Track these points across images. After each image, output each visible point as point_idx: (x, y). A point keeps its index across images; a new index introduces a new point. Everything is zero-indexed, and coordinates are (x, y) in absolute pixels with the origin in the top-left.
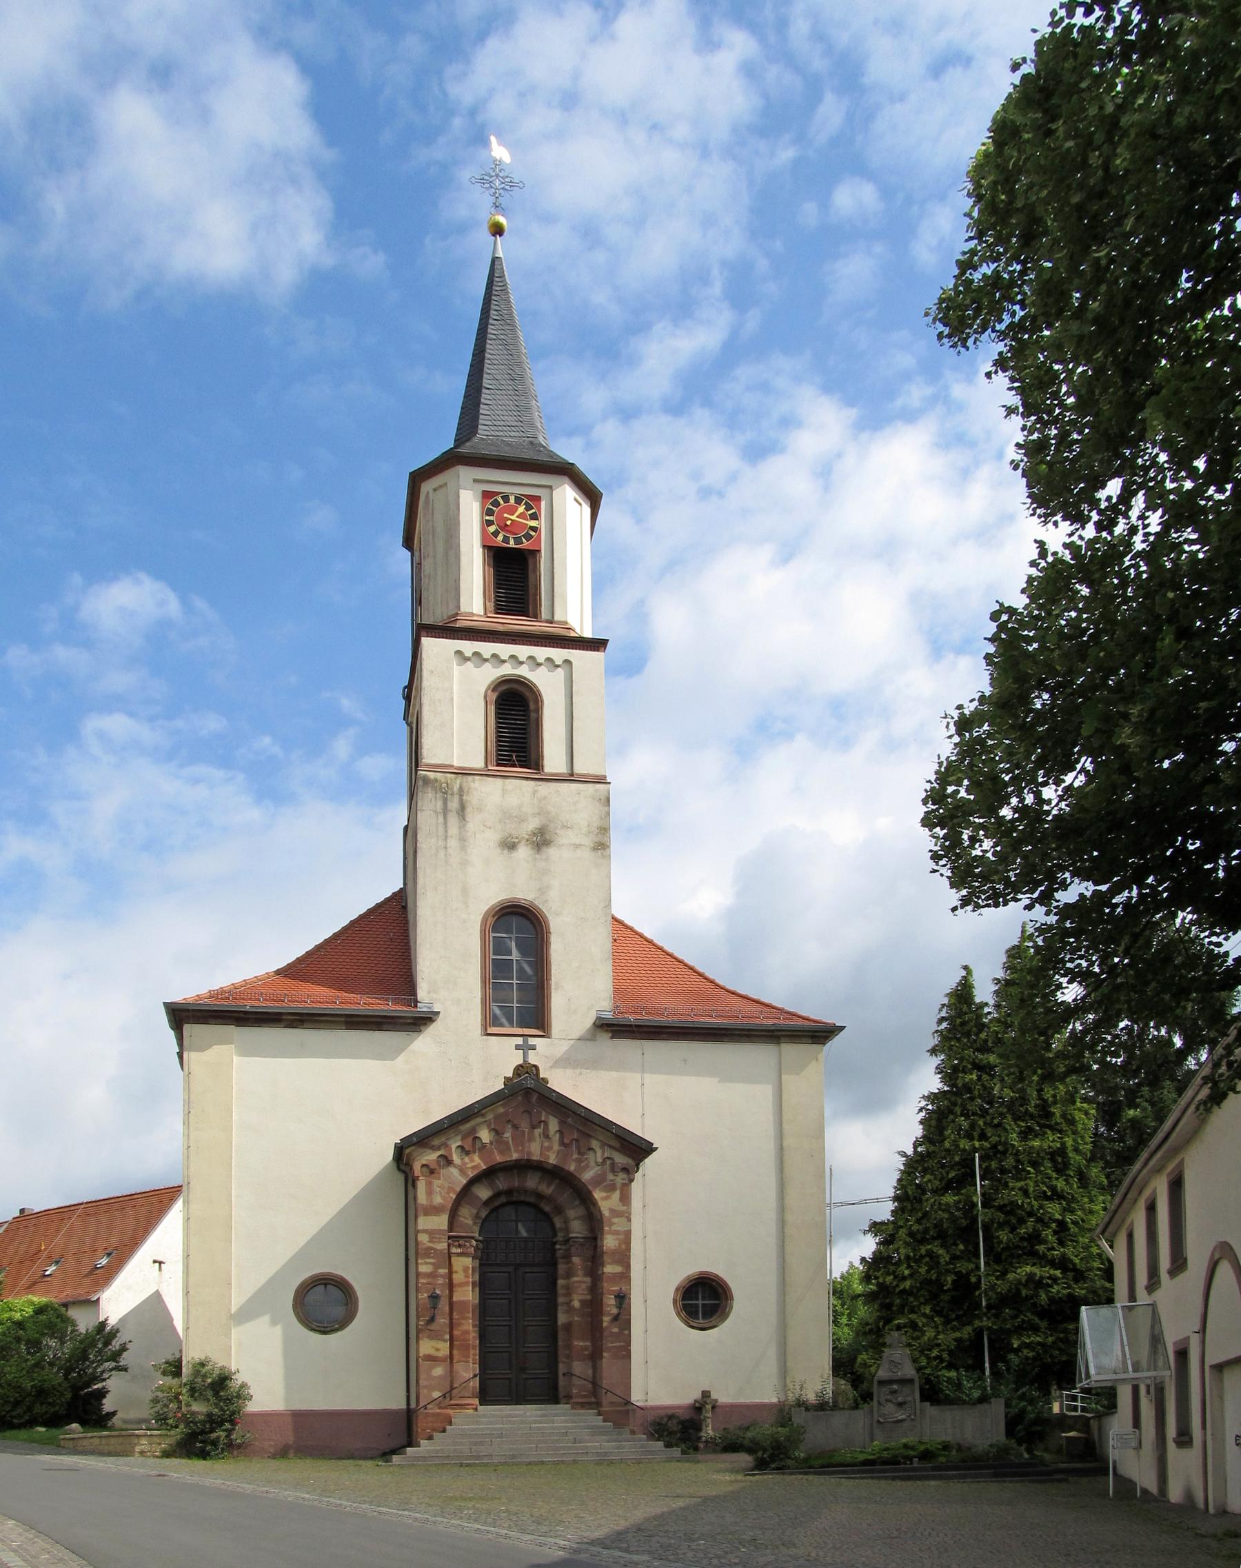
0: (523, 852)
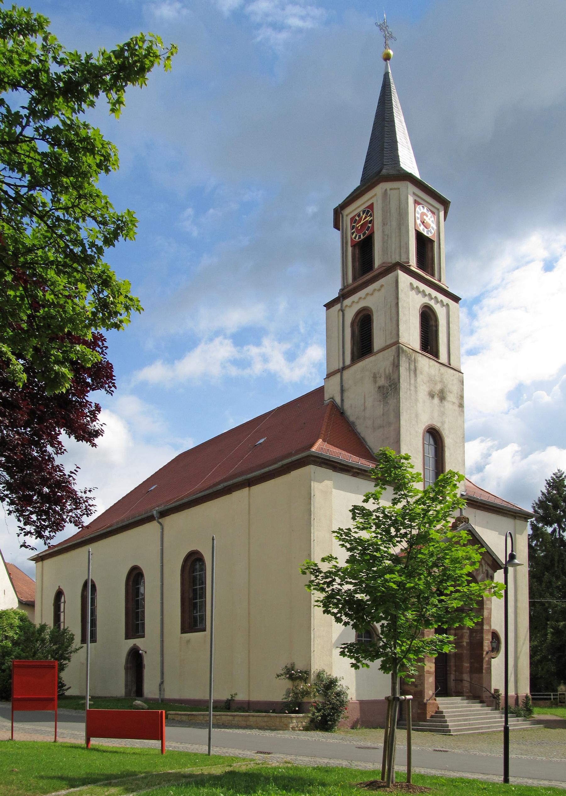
0: (436, 400)
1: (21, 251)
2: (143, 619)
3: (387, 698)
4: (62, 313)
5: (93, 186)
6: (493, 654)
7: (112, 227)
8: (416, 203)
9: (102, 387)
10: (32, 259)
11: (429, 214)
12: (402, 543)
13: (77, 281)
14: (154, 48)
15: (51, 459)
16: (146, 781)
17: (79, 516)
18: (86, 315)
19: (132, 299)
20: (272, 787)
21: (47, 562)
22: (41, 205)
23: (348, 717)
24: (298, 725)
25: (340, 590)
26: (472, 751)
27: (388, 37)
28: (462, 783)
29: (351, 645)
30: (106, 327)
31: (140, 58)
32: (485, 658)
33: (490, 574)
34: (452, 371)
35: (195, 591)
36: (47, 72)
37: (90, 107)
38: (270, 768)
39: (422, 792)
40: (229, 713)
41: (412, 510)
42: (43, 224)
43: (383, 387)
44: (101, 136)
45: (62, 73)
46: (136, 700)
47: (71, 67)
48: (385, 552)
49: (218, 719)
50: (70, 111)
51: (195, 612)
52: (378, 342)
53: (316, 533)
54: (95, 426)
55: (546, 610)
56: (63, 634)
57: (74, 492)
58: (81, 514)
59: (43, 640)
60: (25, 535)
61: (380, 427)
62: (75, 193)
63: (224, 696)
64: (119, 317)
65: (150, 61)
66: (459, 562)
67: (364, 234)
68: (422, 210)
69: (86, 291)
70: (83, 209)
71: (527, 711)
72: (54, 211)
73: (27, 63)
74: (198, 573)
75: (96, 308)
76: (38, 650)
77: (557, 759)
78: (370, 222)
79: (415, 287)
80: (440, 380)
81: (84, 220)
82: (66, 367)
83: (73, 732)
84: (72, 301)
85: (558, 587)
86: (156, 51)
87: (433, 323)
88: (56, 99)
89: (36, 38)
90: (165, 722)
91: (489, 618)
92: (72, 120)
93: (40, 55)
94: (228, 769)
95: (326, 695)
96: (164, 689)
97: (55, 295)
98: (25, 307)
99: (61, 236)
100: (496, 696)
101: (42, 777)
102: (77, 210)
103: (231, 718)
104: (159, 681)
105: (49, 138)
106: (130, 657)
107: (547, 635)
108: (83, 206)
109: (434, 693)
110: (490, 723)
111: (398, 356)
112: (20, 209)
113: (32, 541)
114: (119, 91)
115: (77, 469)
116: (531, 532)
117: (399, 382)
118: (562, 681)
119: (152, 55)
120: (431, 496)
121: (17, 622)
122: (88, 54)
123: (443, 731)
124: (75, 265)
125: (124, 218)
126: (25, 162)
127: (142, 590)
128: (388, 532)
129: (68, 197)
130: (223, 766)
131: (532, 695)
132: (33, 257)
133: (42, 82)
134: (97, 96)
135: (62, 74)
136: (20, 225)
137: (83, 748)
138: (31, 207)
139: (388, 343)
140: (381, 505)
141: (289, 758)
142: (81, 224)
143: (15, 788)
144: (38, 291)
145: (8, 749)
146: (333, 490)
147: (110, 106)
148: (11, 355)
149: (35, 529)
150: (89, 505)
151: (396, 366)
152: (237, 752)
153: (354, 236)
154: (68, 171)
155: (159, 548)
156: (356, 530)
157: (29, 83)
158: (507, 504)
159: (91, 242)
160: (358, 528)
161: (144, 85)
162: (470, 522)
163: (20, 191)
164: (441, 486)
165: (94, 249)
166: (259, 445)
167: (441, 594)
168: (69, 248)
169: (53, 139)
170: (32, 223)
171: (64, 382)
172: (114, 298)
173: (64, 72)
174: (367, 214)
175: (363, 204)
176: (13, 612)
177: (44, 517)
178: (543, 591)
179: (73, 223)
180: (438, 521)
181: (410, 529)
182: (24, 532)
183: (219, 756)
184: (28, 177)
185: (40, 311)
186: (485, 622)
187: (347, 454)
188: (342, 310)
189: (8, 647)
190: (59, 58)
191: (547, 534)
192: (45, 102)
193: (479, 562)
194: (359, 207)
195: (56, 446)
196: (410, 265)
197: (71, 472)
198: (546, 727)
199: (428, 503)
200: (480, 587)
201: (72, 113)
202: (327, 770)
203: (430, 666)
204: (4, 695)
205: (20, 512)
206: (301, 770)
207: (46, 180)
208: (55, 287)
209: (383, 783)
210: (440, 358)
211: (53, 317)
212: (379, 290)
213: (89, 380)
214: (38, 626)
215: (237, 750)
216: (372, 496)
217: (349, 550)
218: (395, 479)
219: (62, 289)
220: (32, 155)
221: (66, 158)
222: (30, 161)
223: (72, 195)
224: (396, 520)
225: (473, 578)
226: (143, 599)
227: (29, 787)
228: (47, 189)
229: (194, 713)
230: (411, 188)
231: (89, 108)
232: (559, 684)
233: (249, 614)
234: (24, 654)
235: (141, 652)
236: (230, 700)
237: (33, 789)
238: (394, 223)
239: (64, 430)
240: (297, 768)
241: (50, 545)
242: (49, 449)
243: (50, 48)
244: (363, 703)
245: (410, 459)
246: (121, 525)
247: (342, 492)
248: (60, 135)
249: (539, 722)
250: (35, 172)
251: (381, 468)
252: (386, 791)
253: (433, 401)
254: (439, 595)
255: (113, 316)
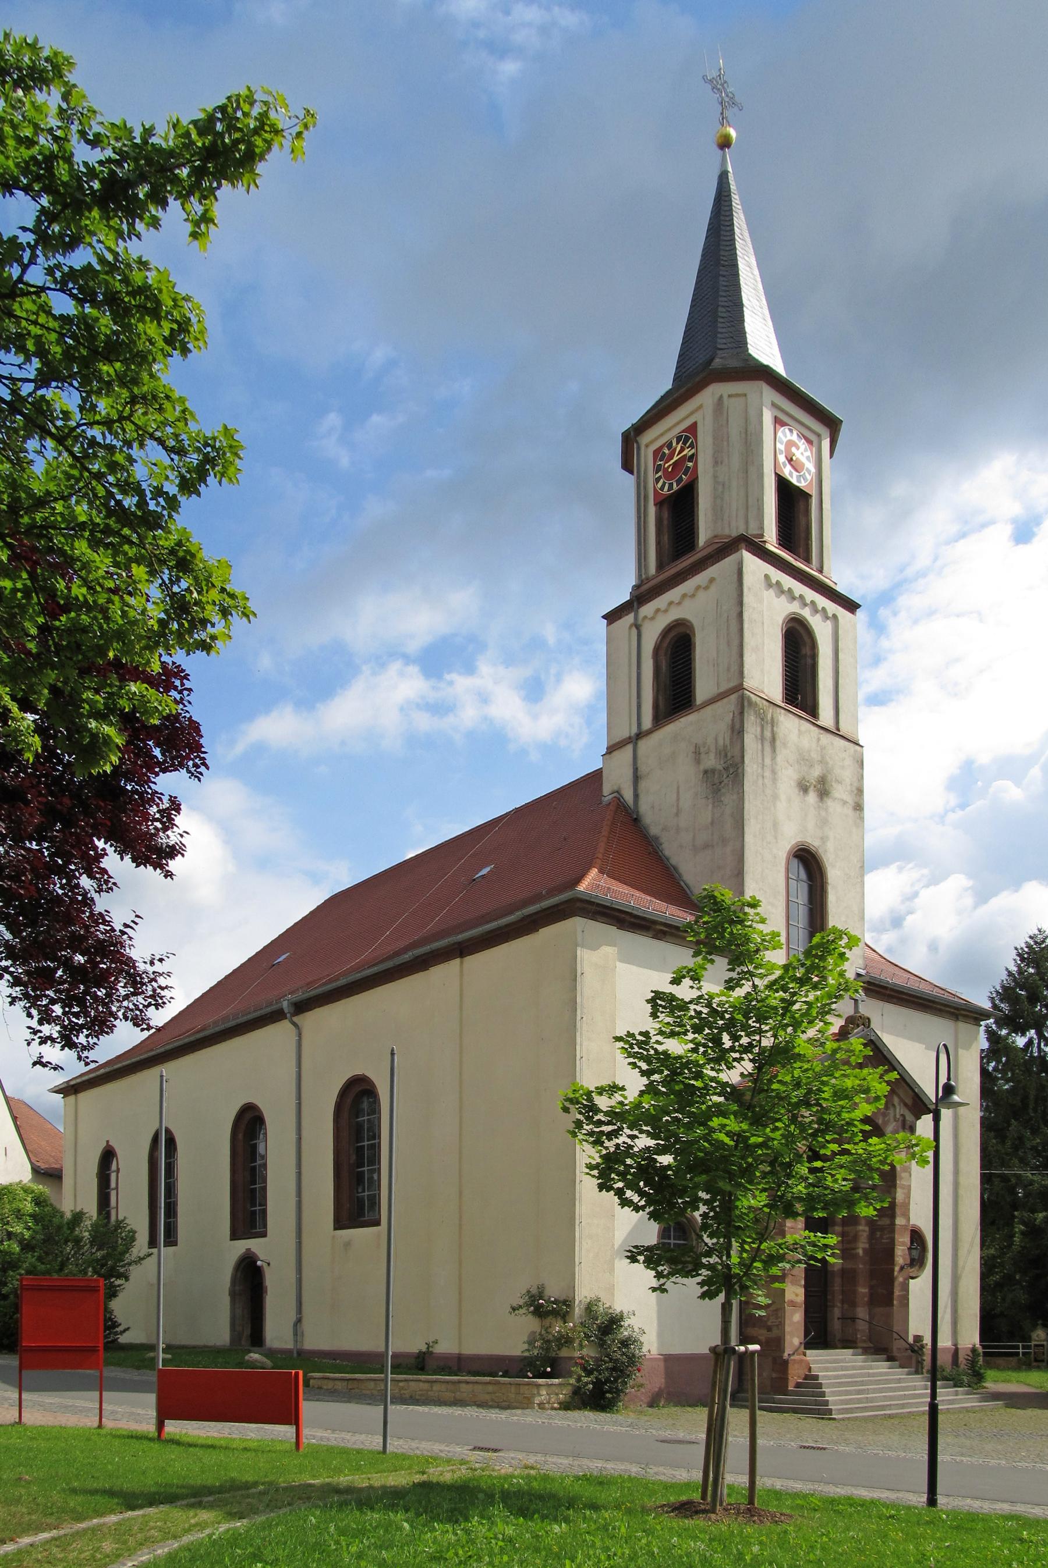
0: (812, 797)
1: (24, 504)
2: (264, 1203)
3: (713, 1350)
4: (102, 621)
5: (158, 379)
6: (913, 1271)
7: (194, 458)
8: (778, 422)
9: (181, 765)
10: (45, 519)
11: (802, 444)
12: (742, 1063)
13: (130, 560)
14: (272, 114)
15: (88, 902)
16: (266, 1499)
17: (141, 1007)
18: (147, 625)
19: (233, 594)
20: (498, 1511)
21: (84, 1096)
22: (61, 416)
23: (642, 1385)
24: (550, 1399)
25: (631, 1147)
26: (870, 1448)
27: (727, 104)
28: (851, 1505)
29: (649, 1249)
30: (186, 648)
31: (245, 135)
32: (897, 1277)
33: (908, 1123)
34: (843, 742)
35: (360, 1150)
36: (68, 159)
37: (151, 228)
38: (496, 1477)
39: (776, 1522)
40: (423, 1377)
41: (763, 1000)
42: (65, 454)
43: (713, 771)
44: (171, 284)
45: (97, 162)
46: (250, 1352)
47: (114, 152)
48: (713, 1079)
49: (402, 1388)
50: (112, 235)
51: (360, 1190)
52: (704, 686)
53: (585, 1043)
54: (168, 837)
55: (1012, 1191)
56: (116, 1230)
57: (130, 962)
58: (146, 1003)
59: (78, 1241)
60: (40, 1044)
61: (707, 846)
62: (125, 394)
63: (415, 1345)
64: (210, 630)
65: (265, 140)
66: (846, 1097)
67: (678, 482)
68: (789, 437)
69: (147, 580)
70: (140, 423)
71: (975, 1376)
72: (84, 427)
73: (30, 143)
74: (366, 1118)
75: (166, 611)
76: (68, 1259)
77: (1027, 1465)
78: (691, 458)
79: (774, 581)
80: (819, 758)
81: (142, 445)
82: (111, 724)
83: (134, 1410)
84: (122, 597)
85: (1034, 1148)
86: (277, 122)
87: (806, 650)
88: (87, 214)
89: (49, 94)
90: (304, 1393)
91: (906, 1205)
92: (116, 255)
93: (55, 128)
94: (418, 1478)
95: (602, 1344)
96: (303, 1333)
97: (90, 588)
98: (34, 610)
99: (99, 476)
100: (916, 1347)
101: (74, 1491)
102: (129, 427)
103: (426, 1386)
104: (293, 1316)
105: (73, 288)
106: (239, 1274)
107: (1012, 1236)
108: (139, 419)
109: (802, 1341)
110: (905, 1397)
111: (742, 713)
112: (21, 424)
113: (53, 1053)
114: (205, 198)
115: (137, 920)
116: (985, 1045)
117: (743, 762)
118: (1040, 1322)
119: (267, 128)
120: (798, 975)
121: (29, 1207)
122: (147, 127)
123: (818, 1412)
124: (126, 531)
125: (217, 441)
126: (29, 333)
127: (261, 1149)
128: (717, 1041)
129: (110, 400)
130: (409, 1474)
131: (984, 1347)
132: (47, 515)
133: (59, 179)
134: (164, 209)
135: (96, 165)
136: (22, 455)
137: (151, 1440)
138: (40, 420)
139: (722, 690)
140: (704, 991)
141: (531, 1460)
142: (135, 452)
143: (24, 1510)
144: (56, 580)
145: (12, 1441)
146: (618, 964)
147: (189, 227)
148: (10, 701)
149: (59, 1032)
150: (160, 987)
151: (738, 731)
152: (437, 1448)
153: (660, 485)
154: (112, 350)
155: (294, 1070)
156: (659, 1038)
157: (34, 182)
158: (943, 992)
159: (155, 488)
160: (661, 1033)
161: (252, 186)
162: (872, 1026)
163: (19, 389)
164: (816, 956)
165: (161, 500)
166: (480, 879)
167: (815, 1156)
168: (115, 499)
169: (81, 289)
170: (43, 450)
171: (109, 753)
172: (199, 593)
173: (102, 160)
174: (685, 443)
175: (678, 423)
176: (22, 1188)
177: (76, 1009)
178: (1007, 1154)
179: (121, 450)
180: (810, 1022)
181: (757, 1038)
182: (39, 1038)
183: (403, 1454)
184: (36, 363)
185: (61, 618)
186: (898, 1211)
187: (643, 896)
188: (637, 626)
189: (13, 1254)
190: (91, 134)
191: (1016, 1048)
192: (66, 219)
193: (885, 1096)
194: (670, 429)
195: (97, 876)
196: (765, 542)
197: (126, 926)
198: (1007, 1406)
199: (792, 988)
200: (889, 1145)
201: (117, 240)
202: (602, 1482)
203: (795, 1292)
204: (5, 1341)
205: (33, 1001)
206: (553, 1480)
207: (69, 368)
208: (89, 572)
209: (704, 1504)
210: (821, 718)
211: (85, 630)
212: (706, 588)
213: (157, 752)
214: (68, 1215)
215: (437, 1444)
216: (688, 973)
217: (643, 1073)
218: (730, 943)
219: (103, 578)
220: (42, 319)
221: (106, 326)
222: (40, 332)
223: (119, 396)
224: (732, 1019)
225: (874, 1127)
226: (265, 1165)
227: (51, 1508)
228: (71, 385)
229: (357, 1376)
230: (769, 394)
231: (148, 230)
232: (1034, 1327)
233: (461, 1193)
234: (43, 1266)
235: (259, 1263)
236: (424, 1353)
237: (57, 1512)
238: (736, 461)
239: (111, 846)
240: (546, 1478)
241: (88, 1061)
242: (85, 882)
243: (75, 114)
244: (669, 1360)
245: (760, 906)
246: (222, 1027)
247: (634, 968)
248: (94, 281)
249: (996, 1396)
250: (49, 353)
251: (705, 923)
252: (710, 1519)
253: (807, 798)
254: (810, 1161)
255: (199, 626)
